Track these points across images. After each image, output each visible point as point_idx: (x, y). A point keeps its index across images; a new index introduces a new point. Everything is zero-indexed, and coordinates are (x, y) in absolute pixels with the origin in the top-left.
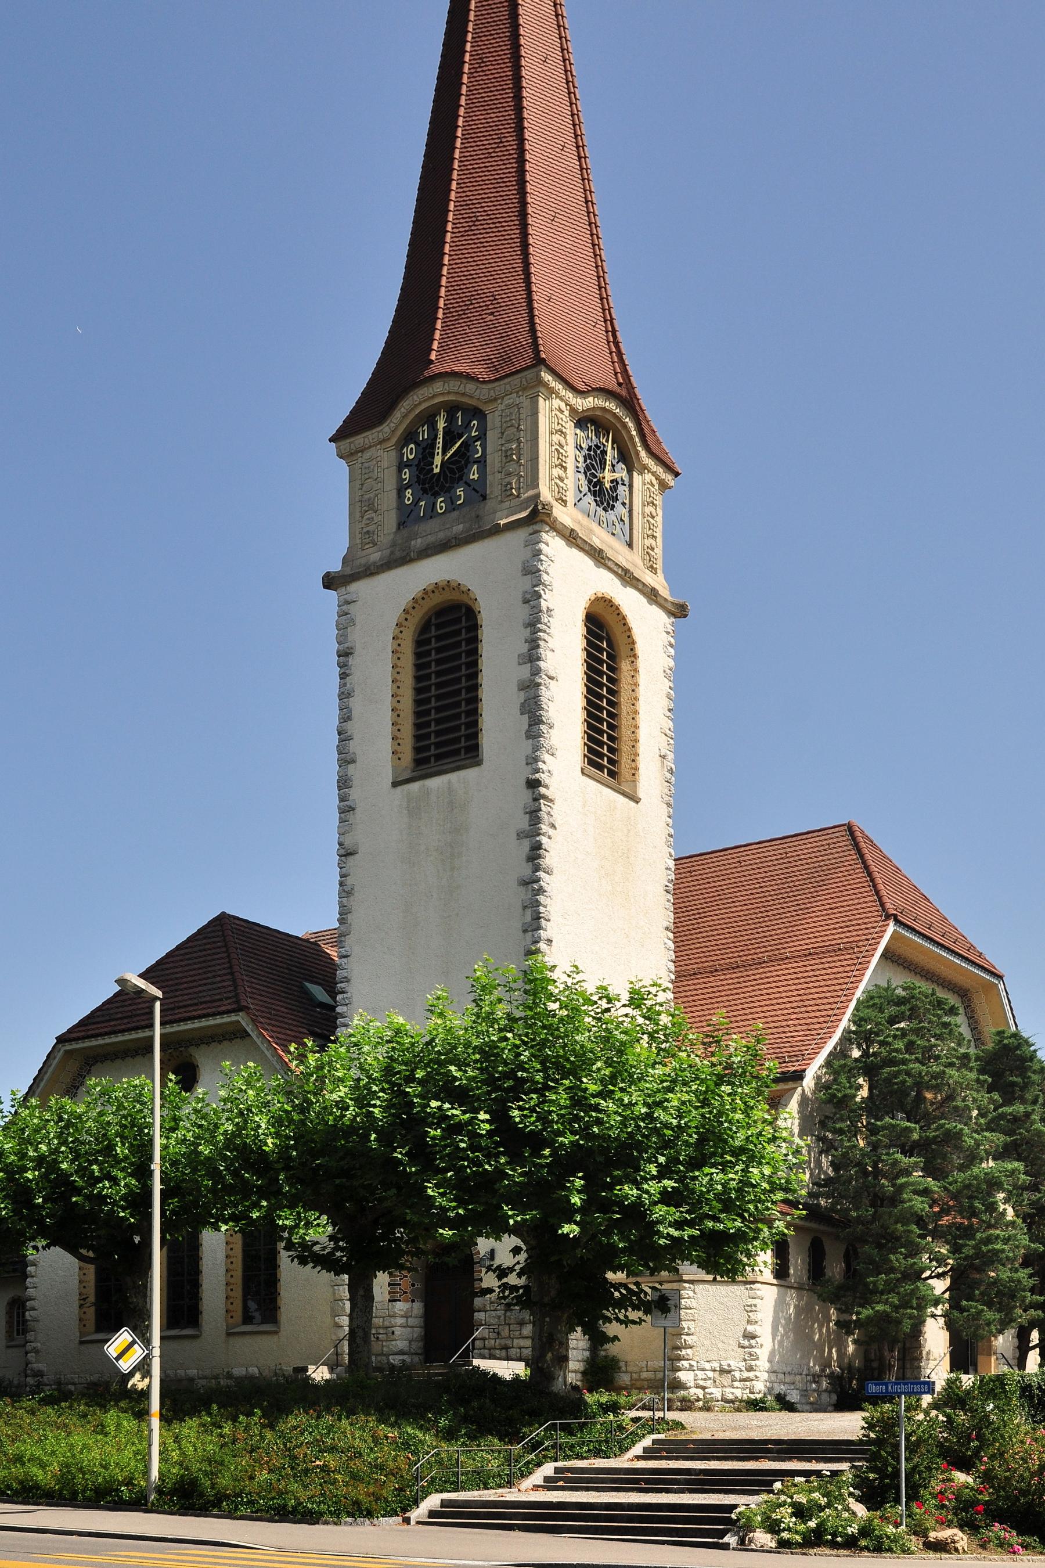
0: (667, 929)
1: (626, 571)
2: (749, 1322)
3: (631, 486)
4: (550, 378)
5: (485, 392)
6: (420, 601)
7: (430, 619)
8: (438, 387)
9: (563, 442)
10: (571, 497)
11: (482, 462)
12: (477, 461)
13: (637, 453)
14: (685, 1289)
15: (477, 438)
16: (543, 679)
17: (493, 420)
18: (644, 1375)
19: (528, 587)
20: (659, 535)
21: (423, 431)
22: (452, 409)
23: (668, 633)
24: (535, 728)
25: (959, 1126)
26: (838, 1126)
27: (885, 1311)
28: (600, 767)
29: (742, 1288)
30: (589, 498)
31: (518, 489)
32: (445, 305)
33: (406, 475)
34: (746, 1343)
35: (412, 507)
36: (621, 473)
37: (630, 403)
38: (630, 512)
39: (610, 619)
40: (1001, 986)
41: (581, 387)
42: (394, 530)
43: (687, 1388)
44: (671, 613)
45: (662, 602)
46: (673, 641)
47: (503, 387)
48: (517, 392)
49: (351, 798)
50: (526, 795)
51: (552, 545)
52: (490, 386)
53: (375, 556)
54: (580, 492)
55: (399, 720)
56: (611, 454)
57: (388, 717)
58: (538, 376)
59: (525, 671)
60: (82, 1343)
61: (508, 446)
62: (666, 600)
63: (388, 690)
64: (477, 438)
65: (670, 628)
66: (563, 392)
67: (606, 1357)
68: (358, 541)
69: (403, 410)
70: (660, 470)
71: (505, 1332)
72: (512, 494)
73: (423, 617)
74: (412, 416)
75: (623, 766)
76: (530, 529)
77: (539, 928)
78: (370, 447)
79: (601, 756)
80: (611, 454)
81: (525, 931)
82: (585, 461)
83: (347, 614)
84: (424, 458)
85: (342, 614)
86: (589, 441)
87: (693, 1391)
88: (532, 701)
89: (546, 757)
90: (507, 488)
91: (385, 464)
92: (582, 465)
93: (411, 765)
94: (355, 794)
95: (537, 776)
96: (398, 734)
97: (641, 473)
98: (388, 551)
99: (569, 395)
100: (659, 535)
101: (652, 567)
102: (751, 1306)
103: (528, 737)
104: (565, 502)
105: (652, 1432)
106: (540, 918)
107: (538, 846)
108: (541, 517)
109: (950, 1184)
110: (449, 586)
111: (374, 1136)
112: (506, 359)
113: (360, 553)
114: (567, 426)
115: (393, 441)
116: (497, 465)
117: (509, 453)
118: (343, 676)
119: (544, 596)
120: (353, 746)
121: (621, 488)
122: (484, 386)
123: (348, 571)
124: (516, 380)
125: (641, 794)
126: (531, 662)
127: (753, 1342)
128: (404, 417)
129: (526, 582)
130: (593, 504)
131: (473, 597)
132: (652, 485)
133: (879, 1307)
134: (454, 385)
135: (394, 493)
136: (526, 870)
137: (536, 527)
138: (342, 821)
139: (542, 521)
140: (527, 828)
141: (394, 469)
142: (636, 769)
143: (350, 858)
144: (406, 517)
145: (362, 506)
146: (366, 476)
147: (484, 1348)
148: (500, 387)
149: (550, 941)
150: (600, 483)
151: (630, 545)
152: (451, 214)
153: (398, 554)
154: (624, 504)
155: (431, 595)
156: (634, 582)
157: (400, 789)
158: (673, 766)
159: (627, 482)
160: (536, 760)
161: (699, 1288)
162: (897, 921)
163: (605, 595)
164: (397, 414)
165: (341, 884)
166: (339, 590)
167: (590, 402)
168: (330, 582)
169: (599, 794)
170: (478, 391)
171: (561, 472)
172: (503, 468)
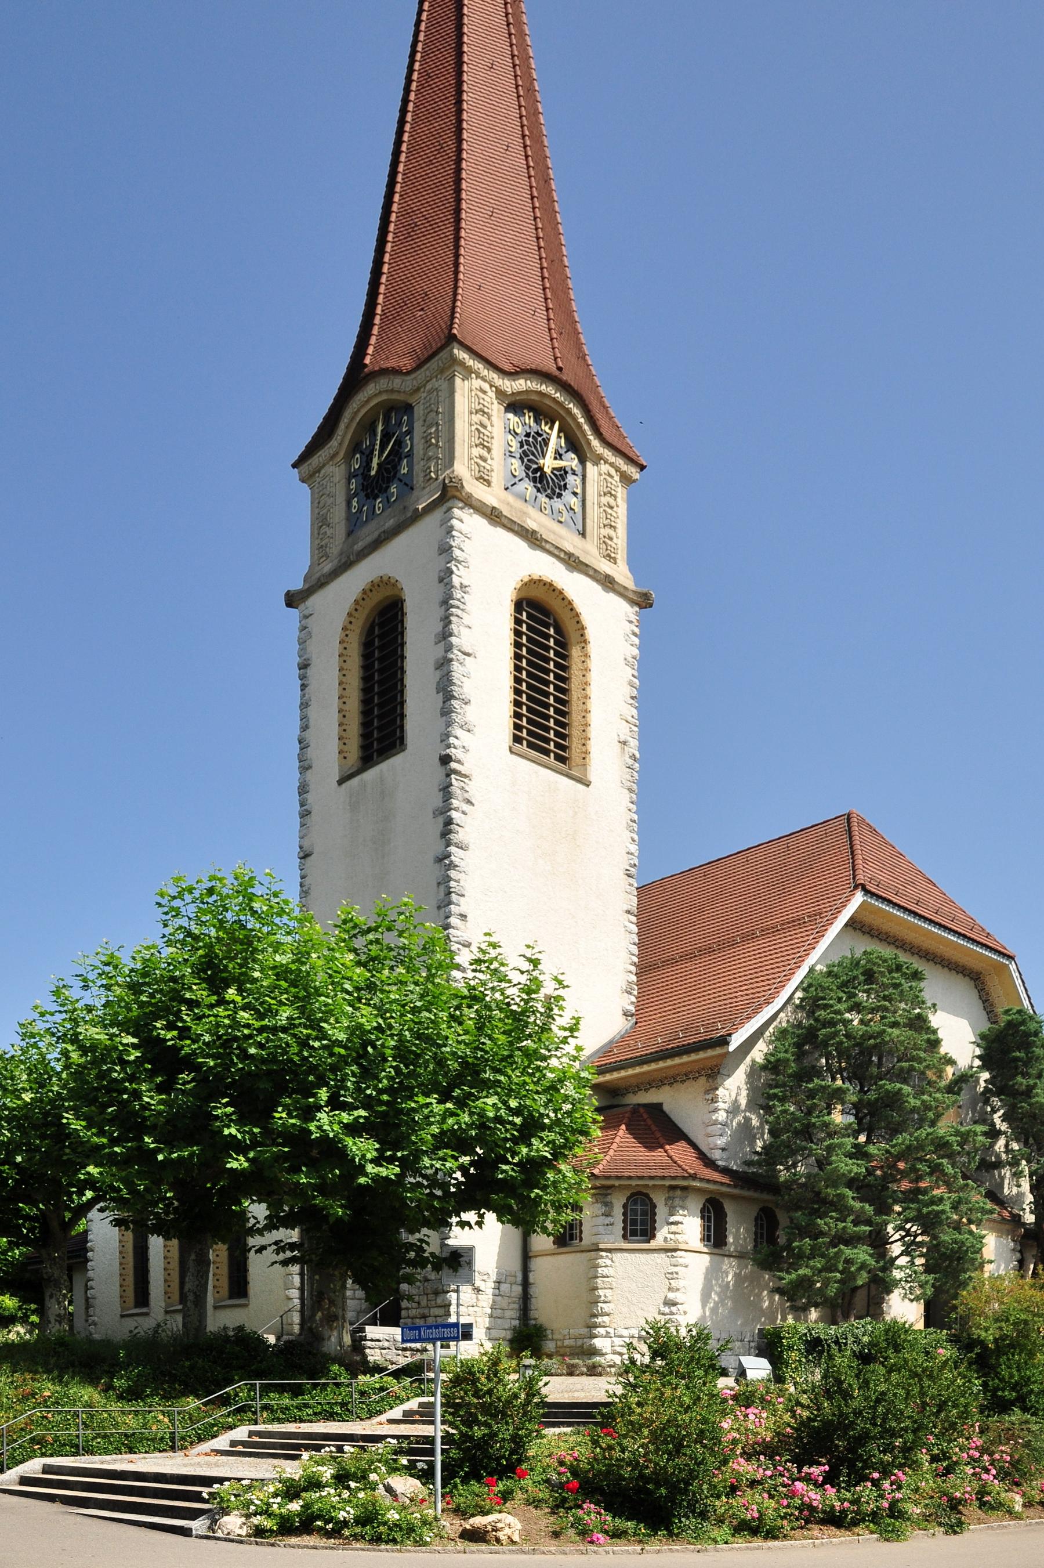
0: (628, 912)
1: (570, 555)
2: (670, 1289)
7: (374, 621)
9: (613, 503)
10: (498, 479)
14: (602, 1257)
16: (455, 654)
17: (419, 411)
18: (567, 1343)
19: (442, 566)
23: (631, 622)
25: (898, 1085)
26: (772, 1091)
27: (805, 1275)
29: (663, 1255)
31: (436, 472)
34: (667, 1310)
36: (571, 461)
40: (1013, 967)
41: (507, 367)
43: (603, 1355)
44: (633, 602)
45: (622, 590)
51: (467, 525)
52: (413, 376)
55: (345, 721)
58: (452, 354)
59: (439, 651)
60: (122, 1316)
65: (633, 618)
67: (535, 1325)
70: (620, 462)
71: (424, 1303)
72: (431, 478)
73: (367, 619)
74: (354, 425)
75: (573, 751)
76: (444, 508)
77: (450, 903)
80: (555, 440)
81: (439, 908)
83: (306, 628)
85: (303, 628)
87: (609, 1357)
96: (344, 734)
97: (596, 463)
99: (493, 376)
101: (609, 556)
102: (672, 1273)
104: (615, 559)
105: (418, 1396)
106: (450, 893)
107: (449, 822)
108: (450, 494)
109: (893, 1146)
111: (127, 1084)
113: (317, 568)
115: (342, 454)
118: (303, 687)
120: (310, 752)
121: (570, 479)
122: (408, 378)
125: (593, 775)
127: (674, 1309)
128: (347, 427)
132: (612, 477)
133: (801, 1272)
136: (439, 847)
138: (302, 825)
140: (441, 805)
142: (587, 752)
143: (309, 859)
145: (320, 522)
147: (408, 1317)
149: (463, 917)
150: (540, 469)
151: (583, 534)
152: (392, 225)
157: (344, 785)
160: (448, 735)
161: (617, 1256)
162: (867, 892)
165: (301, 885)
167: (521, 384)
168: (292, 600)
169: (536, 776)
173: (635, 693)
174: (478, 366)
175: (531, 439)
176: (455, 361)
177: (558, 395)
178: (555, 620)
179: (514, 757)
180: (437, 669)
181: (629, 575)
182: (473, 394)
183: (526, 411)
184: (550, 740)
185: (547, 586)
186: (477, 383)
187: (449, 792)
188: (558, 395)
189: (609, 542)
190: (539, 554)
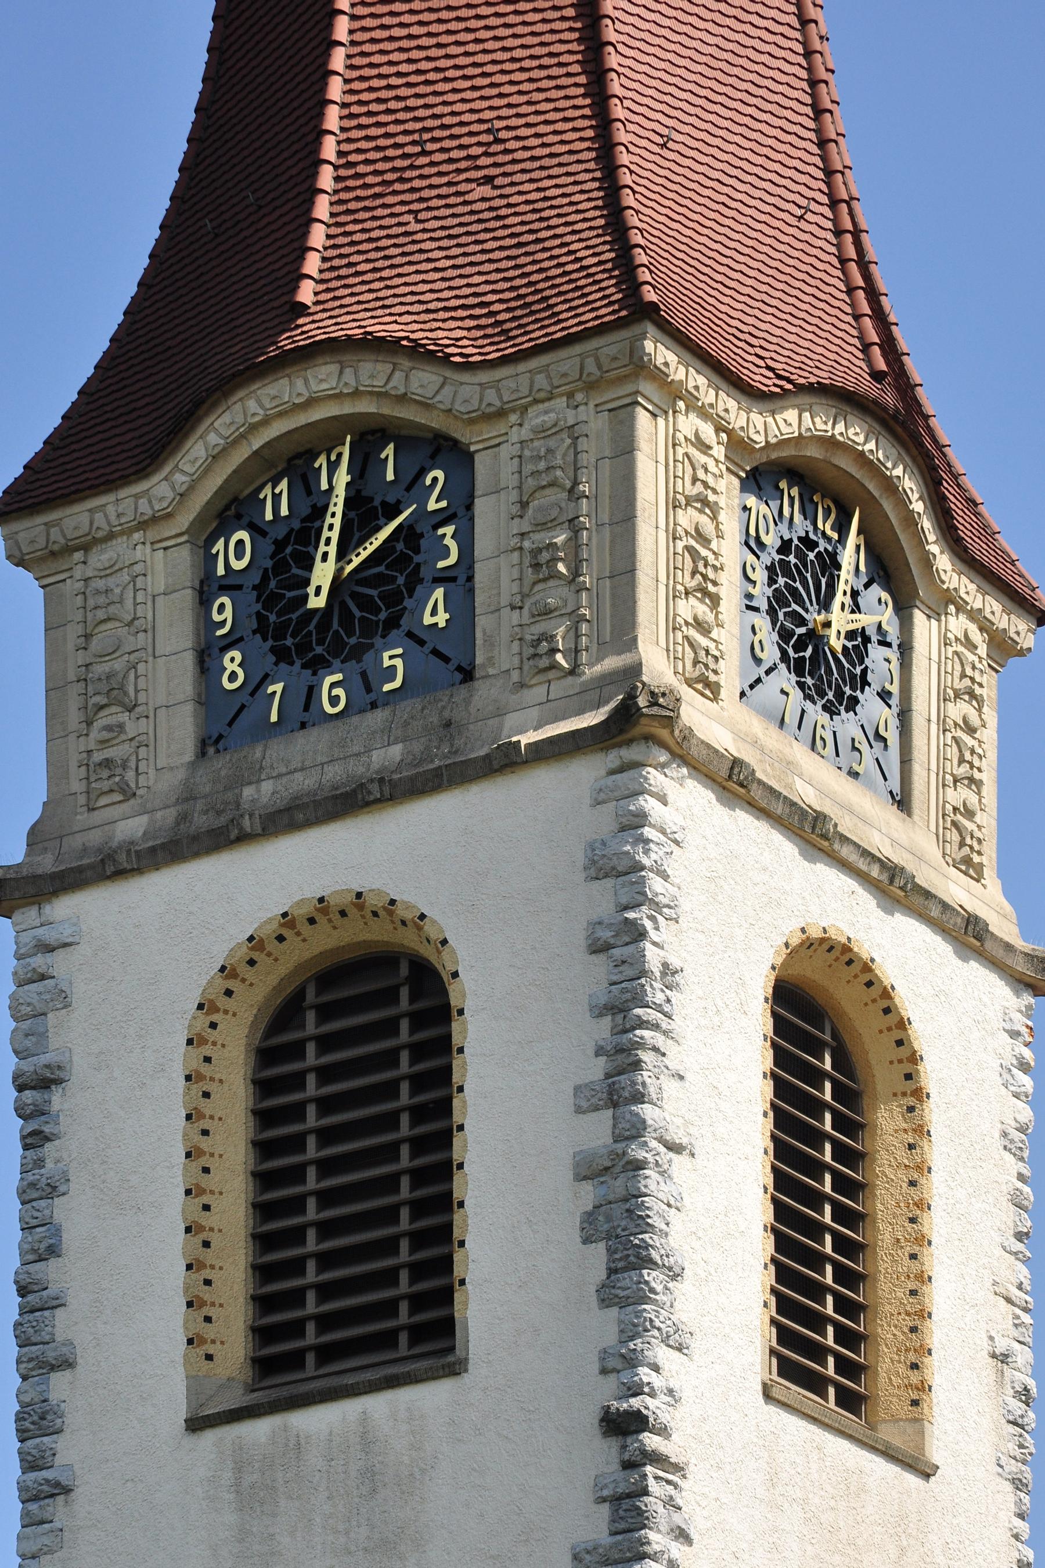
1: (893, 871)
3: (905, 649)
4: (672, 358)
5: (468, 392)
6: (272, 946)
7: (299, 994)
8: (323, 377)
9: (708, 528)
10: (731, 675)
11: (460, 581)
12: (444, 578)
13: (927, 562)
15: (445, 518)
17: (495, 469)
20: (988, 777)
21: (276, 498)
22: (369, 438)
23: (1014, 1034)
24: (627, 1279)
28: (815, 1384)
30: (784, 678)
32: (340, 154)
33: (225, 612)
35: (244, 698)
36: (878, 612)
37: (903, 420)
38: (904, 716)
39: (844, 996)
42: (189, 756)
44: (1022, 983)
45: (1000, 953)
46: (1028, 1054)
47: (524, 381)
48: (570, 395)
49: (58, 1460)
50: (603, 1455)
51: (678, 803)
52: (484, 377)
53: (131, 827)
54: (758, 661)
56: (850, 556)
57: (172, 1248)
59: (596, 1131)
61: (542, 538)
62: (1009, 947)
63: (172, 1176)
64: (445, 518)
65: (1020, 1022)
66: (708, 396)
68: (77, 786)
69: (213, 438)
70: (993, 607)
72: (554, 666)
73: (277, 989)
76: (612, 758)
78: (111, 536)
79: (818, 1352)
80: (850, 556)
82: (772, 581)
83: (43, 977)
84: (280, 566)
86: (783, 528)
88: (618, 1209)
89: (662, 1354)
90: (538, 654)
91: (158, 582)
92: (762, 593)
93: (247, 1374)
94: (69, 1451)
95: (635, 1402)
97: (935, 614)
98: (171, 814)
99: (728, 404)
100: (988, 777)
101: (967, 861)
103: (605, 1302)
104: (979, 868)
108: (644, 727)
110: (361, 907)
112: (532, 304)
113: (83, 818)
114: (721, 485)
115: (184, 520)
116: (508, 589)
117: (545, 556)
118: (34, 1140)
119: (653, 934)
120: (63, 1325)
121: (876, 653)
122: (466, 377)
123: (47, 864)
124: (566, 361)
125: (936, 1453)
126: (615, 1105)
129: (601, 900)
130: (796, 694)
131: (434, 935)
132: (972, 647)
134: (372, 372)
135: (189, 660)
137: (628, 754)
138: (29, 1521)
139: (649, 738)
141: (187, 597)
142: (924, 1388)
144: (225, 724)
146: (101, 614)
148: (515, 381)
150: (815, 638)
151: (903, 802)
153: (201, 821)
154: (884, 695)
155: (306, 929)
156: (918, 900)
157: (210, 1437)
158: (1032, 1384)
159: (893, 637)
160: (632, 1361)
163: (832, 934)
164: (195, 451)
166: (17, 916)
167: (789, 422)
169: (810, 1449)
170: (447, 390)
171: (703, 610)
172: (524, 596)
173: (1026, 1224)
174: (696, 380)
175: (792, 559)
176: (640, 367)
177: (871, 445)
178: (835, 1035)
179: (772, 1409)
180: (581, 1177)
181: (1008, 908)
182: (680, 451)
183: (783, 485)
184: (826, 1350)
185: (835, 953)
186: (689, 424)
187: (640, 1512)
188: (871, 445)
189: (969, 825)
190: (827, 874)
